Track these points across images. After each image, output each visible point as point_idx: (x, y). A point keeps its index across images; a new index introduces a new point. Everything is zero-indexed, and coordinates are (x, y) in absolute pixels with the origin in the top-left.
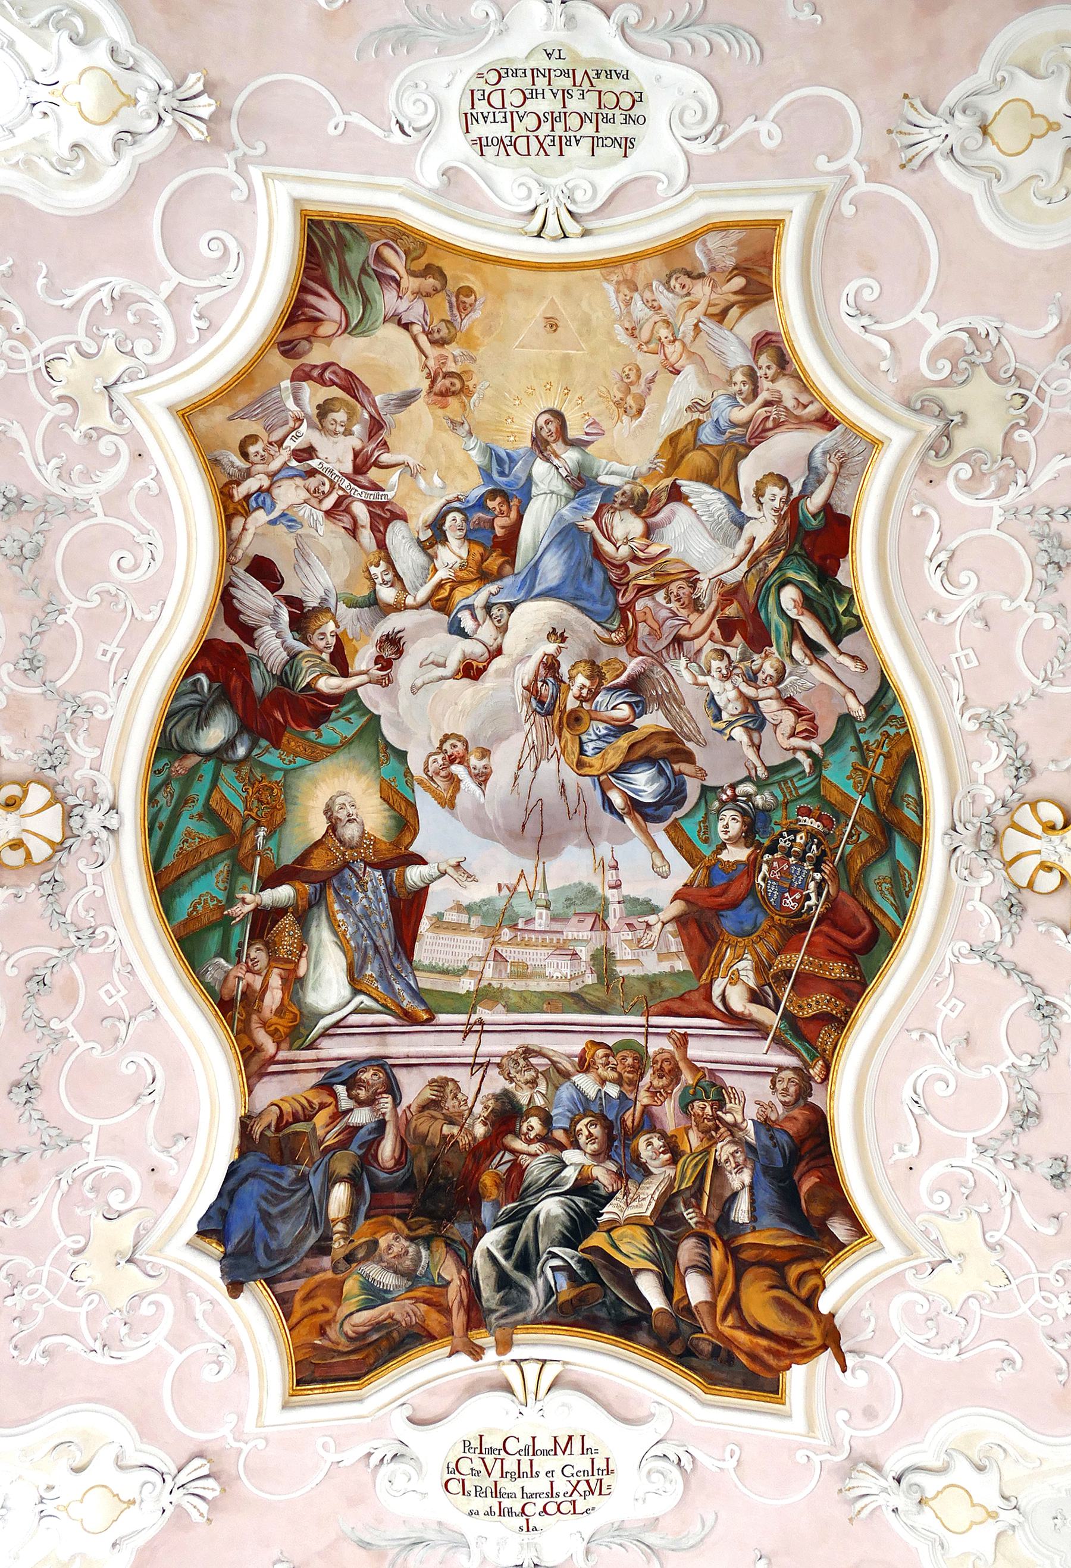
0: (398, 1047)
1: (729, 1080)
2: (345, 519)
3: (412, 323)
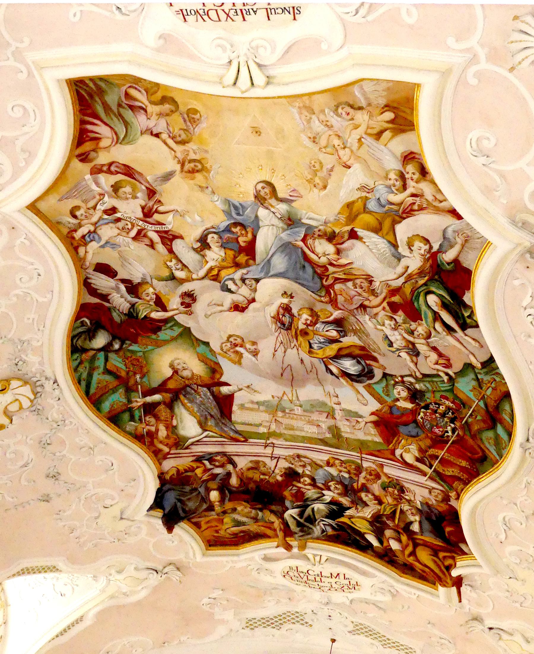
0: (231, 449)
2: (145, 240)
3: (161, 133)
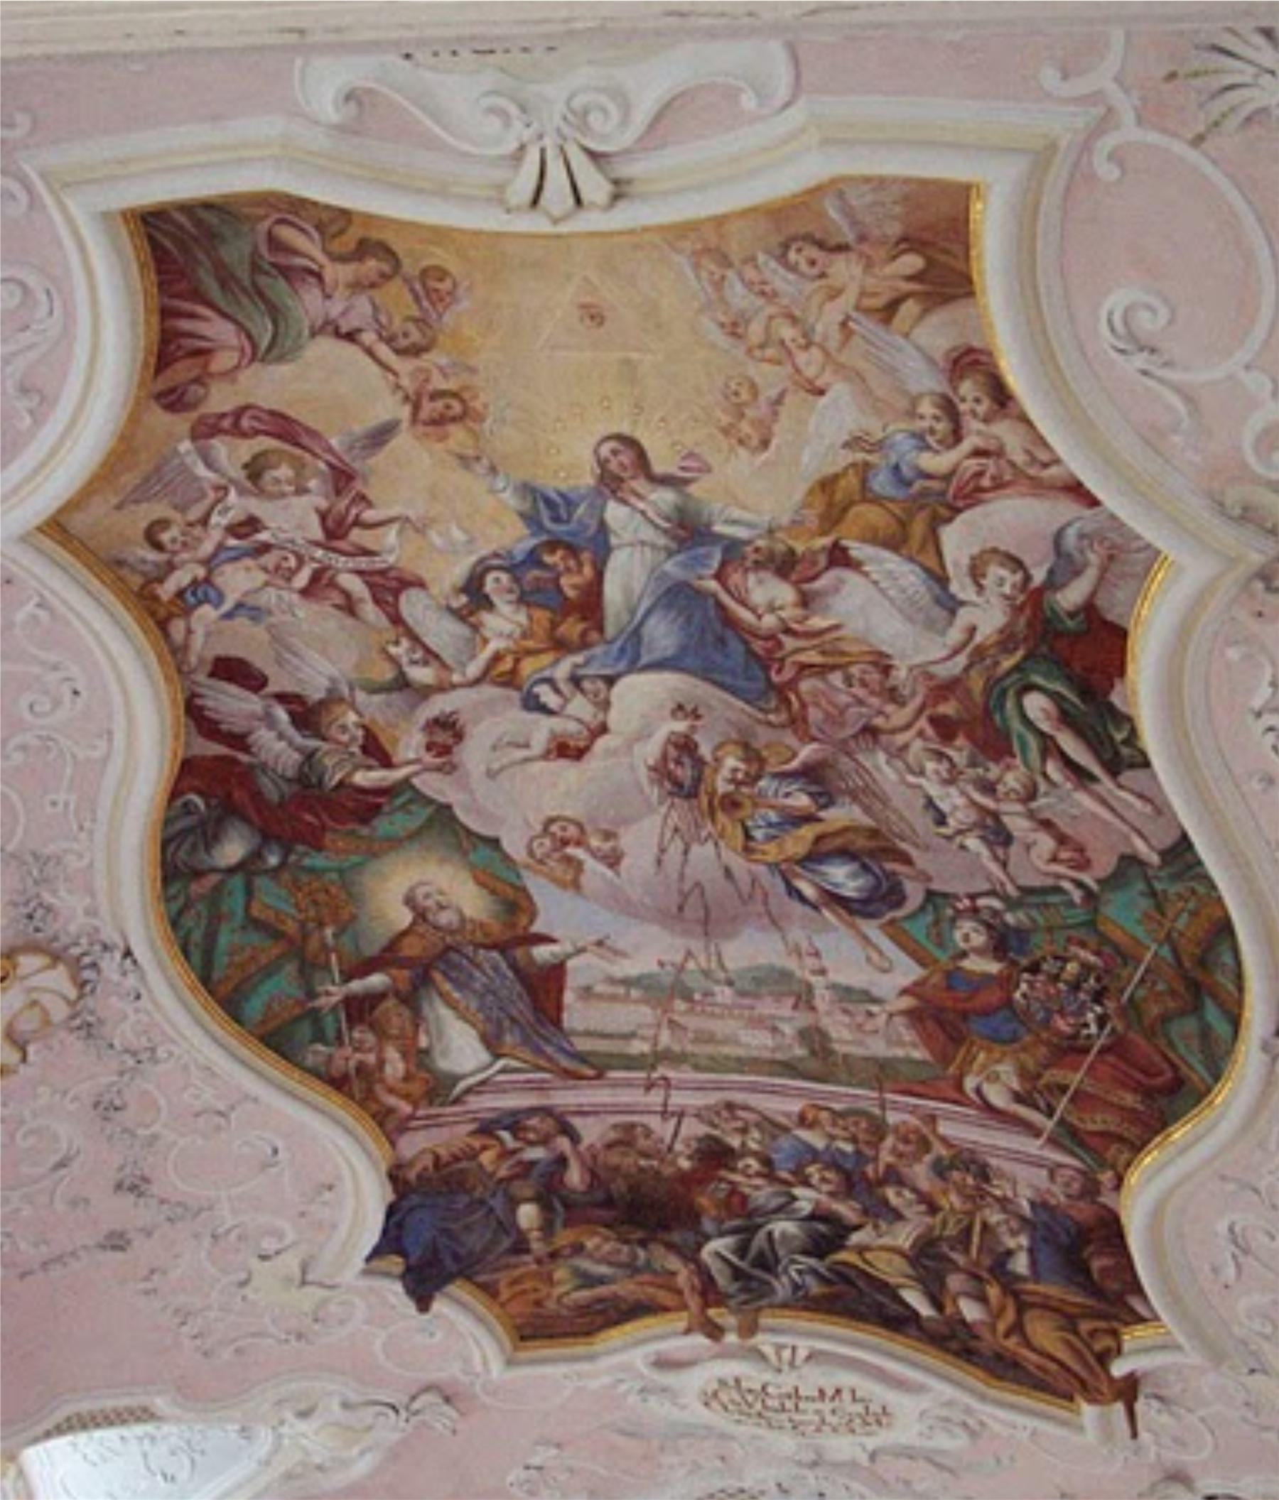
0: (565, 1098)
1: (994, 1162)
3: (359, 330)
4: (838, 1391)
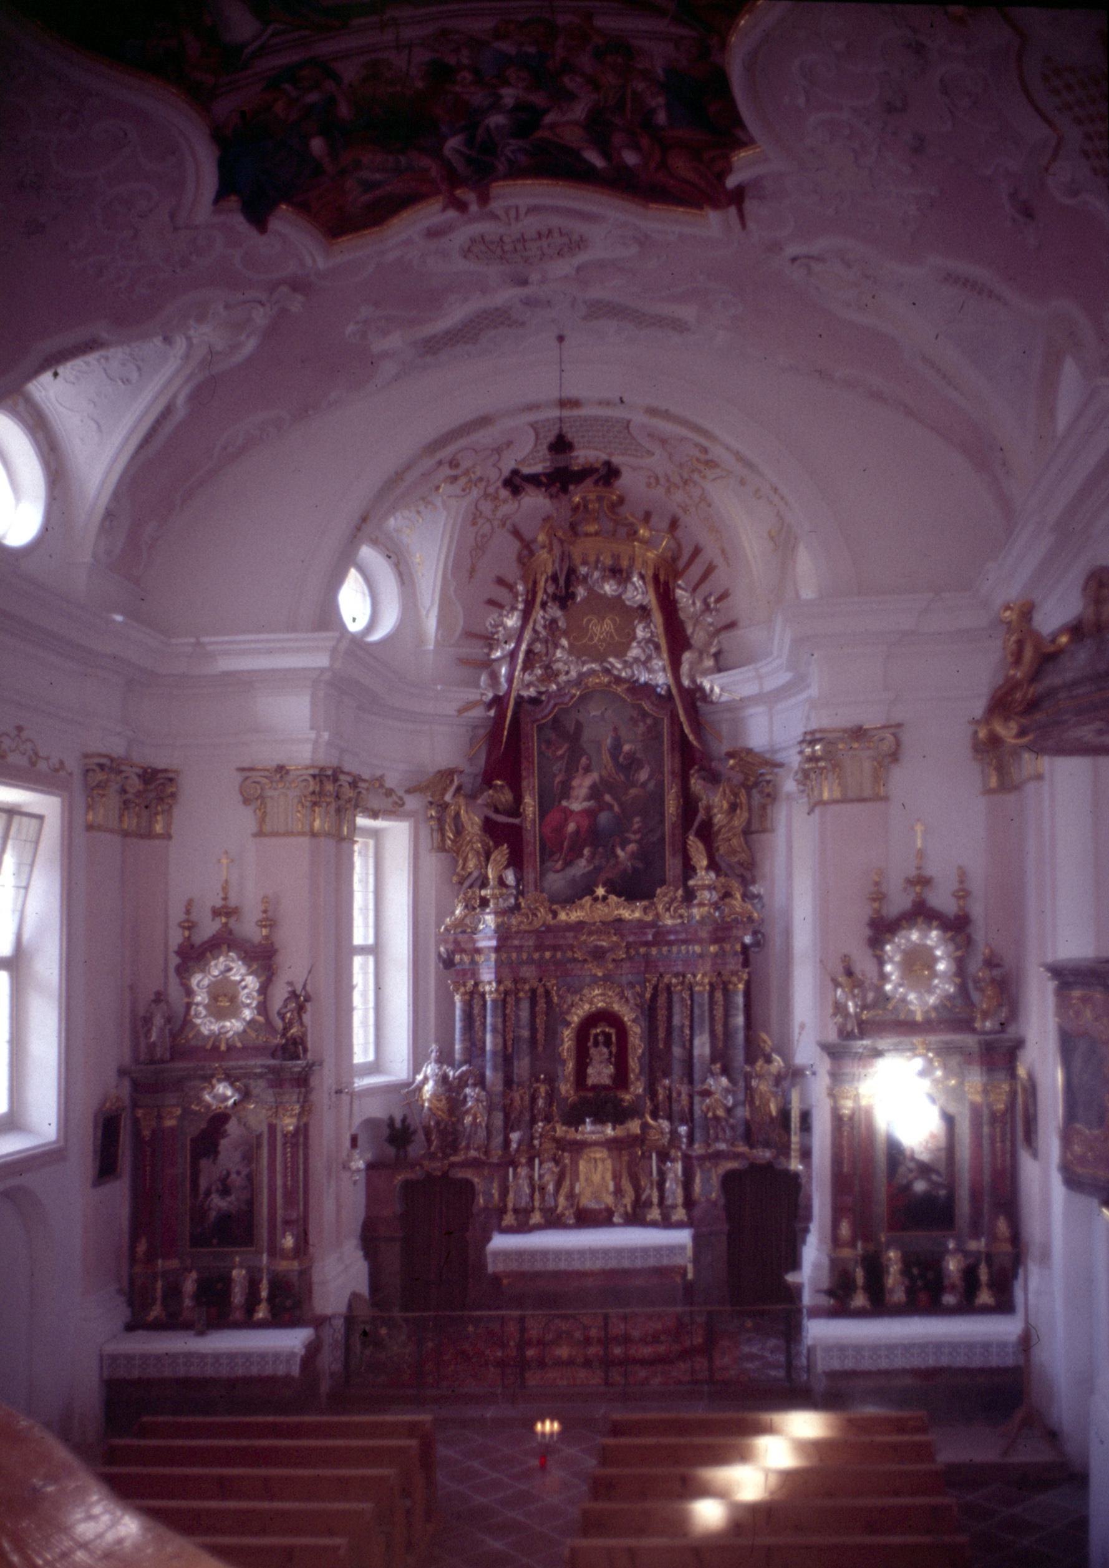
4: (550, 231)
